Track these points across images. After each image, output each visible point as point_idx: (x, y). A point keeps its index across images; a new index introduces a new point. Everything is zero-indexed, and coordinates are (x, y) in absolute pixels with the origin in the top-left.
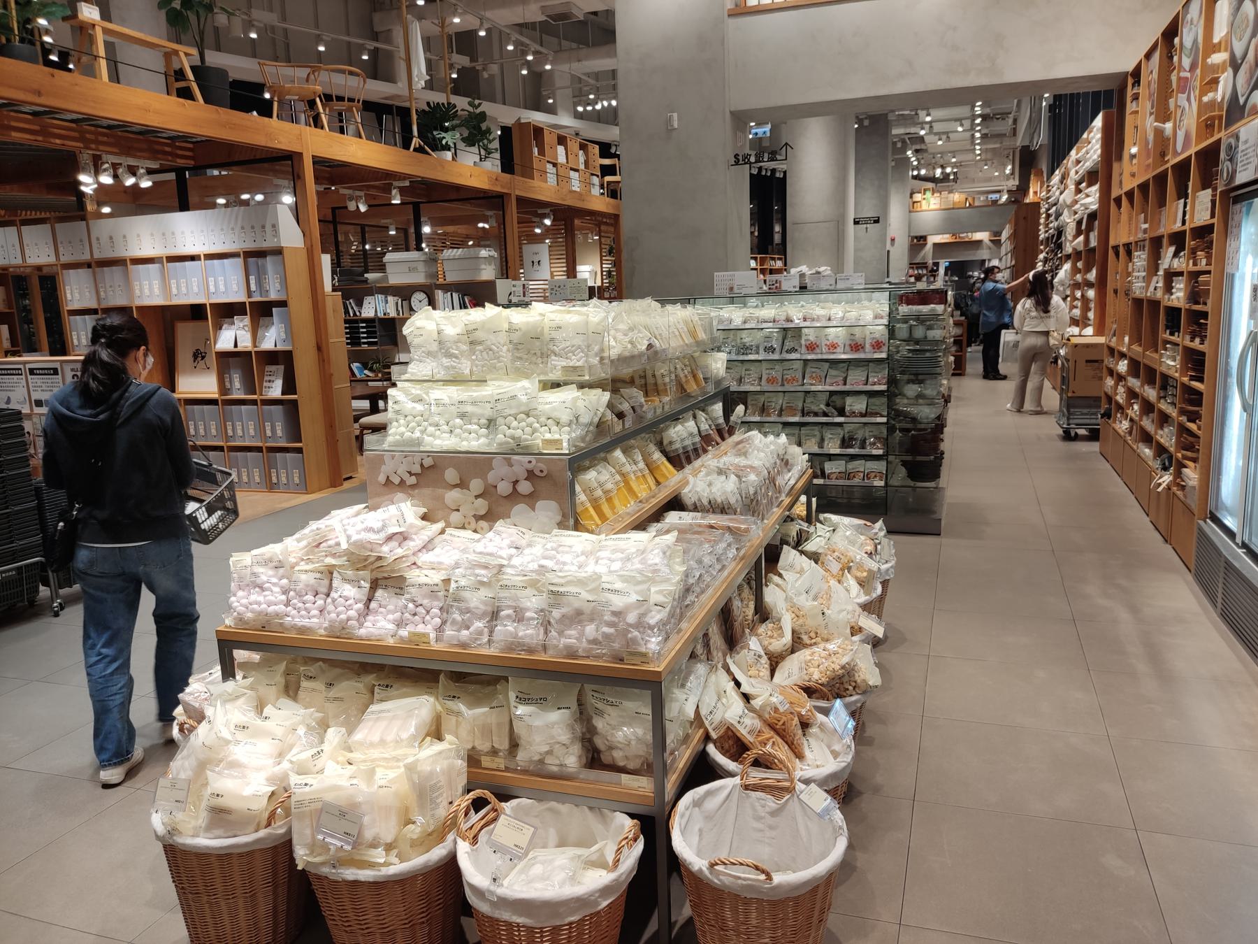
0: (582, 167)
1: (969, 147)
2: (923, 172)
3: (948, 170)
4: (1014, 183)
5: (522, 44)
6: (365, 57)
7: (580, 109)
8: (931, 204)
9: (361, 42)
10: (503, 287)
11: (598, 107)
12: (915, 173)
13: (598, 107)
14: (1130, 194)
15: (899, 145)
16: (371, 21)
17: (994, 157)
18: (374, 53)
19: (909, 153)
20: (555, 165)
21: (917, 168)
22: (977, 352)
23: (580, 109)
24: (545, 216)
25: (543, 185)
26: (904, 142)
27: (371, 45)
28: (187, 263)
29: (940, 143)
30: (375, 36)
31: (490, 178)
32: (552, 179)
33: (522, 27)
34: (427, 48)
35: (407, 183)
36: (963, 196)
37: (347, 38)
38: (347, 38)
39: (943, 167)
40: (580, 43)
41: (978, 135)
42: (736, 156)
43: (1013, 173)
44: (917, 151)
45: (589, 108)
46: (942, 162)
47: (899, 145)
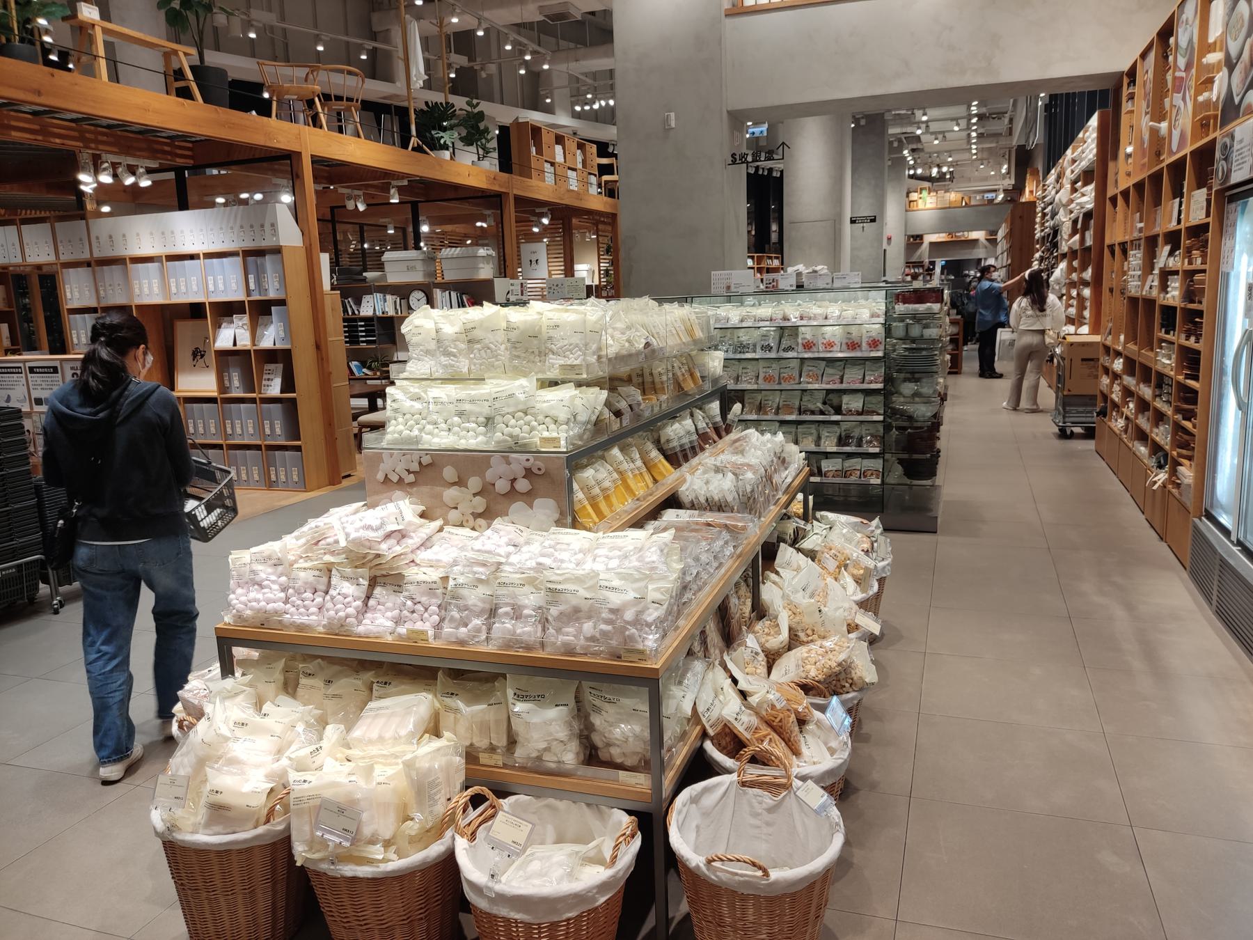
0: (580, 166)
1: (965, 146)
2: (919, 171)
3: (945, 169)
4: (1010, 182)
5: (520, 44)
6: (364, 57)
7: (578, 108)
8: (927, 203)
9: (359, 41)
10: (501, 286)
11: (596, 106)
12: (912, 172)
13: (596, 106)
14: (1125, 194)
15: (896, 144)
16: (370, 21)
17: (990, 156)
18: (373, 53)
19: (906, 152)
20: (553, 164)
21: (914, 167)
22: (973, 350)
23: (578, 108)
24: (542, 215)
25: (541, 184)
26: (900, 141)
27: (370, 45)
28: (186, 262)
29: (936, 142)
30: (374, 36)
31: (488, 177)
32: (549, 178)
33: (520, 27)
34: (426, 48)
35: (405, 183)
36: (959, 196)
37: (346, 38)
38: (346, 38)
39: (939, 166)
40: (577, 43)
41: (974, 134)
43: (1008, 173)
44: (913, 150)
45: (587, 108)
46: (938, 161)
47: (896, 144)
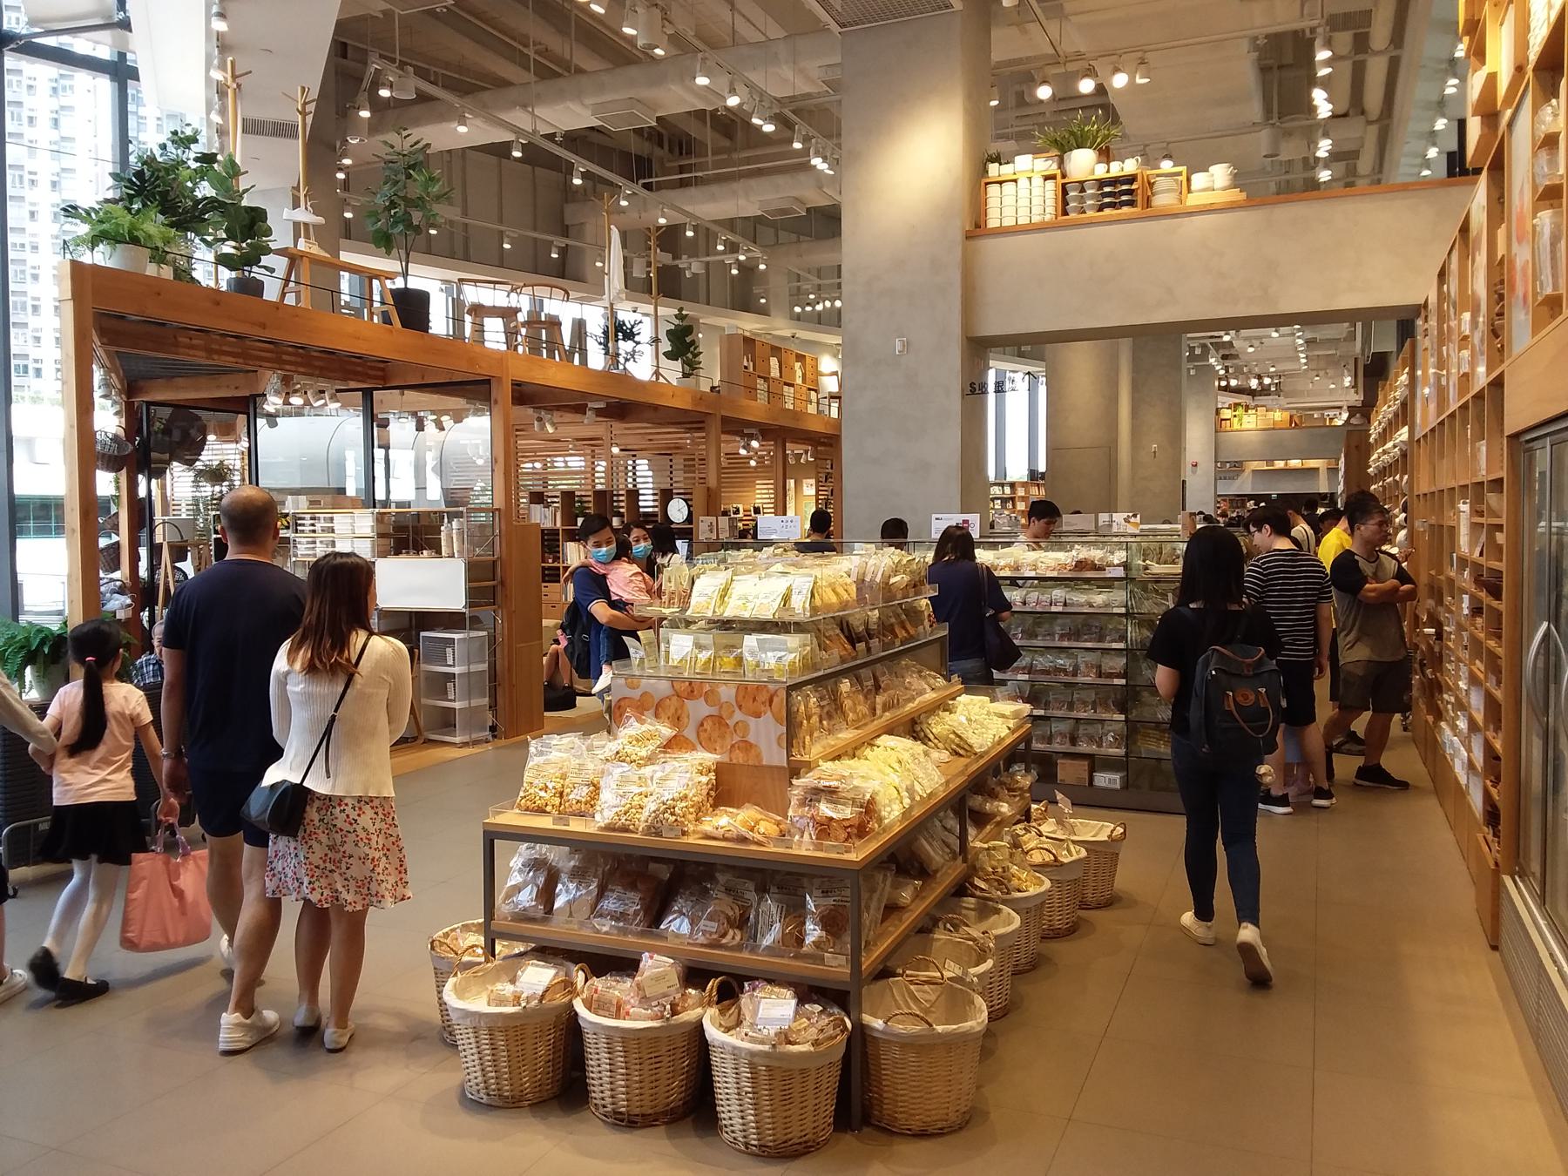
0: (799, 381)
1: (1291, 354)
2: (1233, 383)
3: (1267, 381)
4: (1356, 398)
5: (733, 243)
6: (555, 256)
7: (798, 309)
8: (1249, 423)
9: (550, 238)
10: (704, 528)
11: (819, 307)
12: (1223, 383)
13: (819, 307)
14: (1425, 436)
15: (1198, 351)
16: (562, 212)
17: (1325, 365)
18: (564, 251)
19: (1212, 361)
20: (766, 379)
21: (1226, 378)
22: (421, 488)
23: (798, 309)
24: (751, 437)
25: (753, 403)
26: (1204, 346)
27: (561, 242)
28: (298, 486)
29: (1251, 350)
30: (565, 231)
31: (693, 399)
32: (762, 397)
33: (730, 224)
34: (624, 245)
35: (602, 405)
36: (1286, 415)
37: (535, 235)
38: (535, 235)
39: (1259, 377)
40: (799, 234)
41: (1300, 341)
42: (972, 384)
43: (1355, 386)
44: (1225, 357)
45: (809, 309)
46: (1257, 370)
47: (1198, 351)
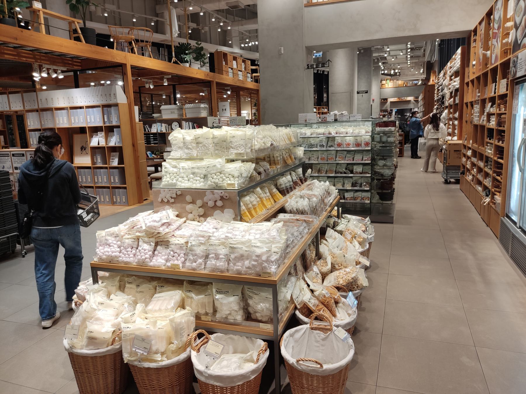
0: (243, 70)
1: (405, 61)
2: (386, 72)
3: (397, 71)
4: (424, 76)
5: (218, 18)
6: (153, 24)
7: (243, 45)
8: (389, 85)
9: (151, 17)
10: (210, 120)
11: (250, 45)
12: (383, 72)
13: (250, 45)
14: (472, 81)
15: (376, 61)
16: (155, 9)
17: (416, 65)
18: (157, 22)
19: (380, 64)
20: (232, 69)
21: (384, 70)
22: (408, 147)
23: (243, 45)
24: (228, 90)
25: (227, 77)
26: (378, 59)
27: (155, 19)
28: (78, 110)
29: (393, 60)
30: (157, 15)
31: (205, 74)
32: (231, 75)
33: (218, 11)
34: (179, 20)
35: (170, 77)
36: (403, 82)
37: (145, 16)
38: (145, 16)
39: (394, 70)
40: (242, 18)
41: (409, 56)
42: (308, 65)
43: (423, 72)
44: (383, 63)
45: (246, 45)
46: (394, 67)
47: (376, 61)
